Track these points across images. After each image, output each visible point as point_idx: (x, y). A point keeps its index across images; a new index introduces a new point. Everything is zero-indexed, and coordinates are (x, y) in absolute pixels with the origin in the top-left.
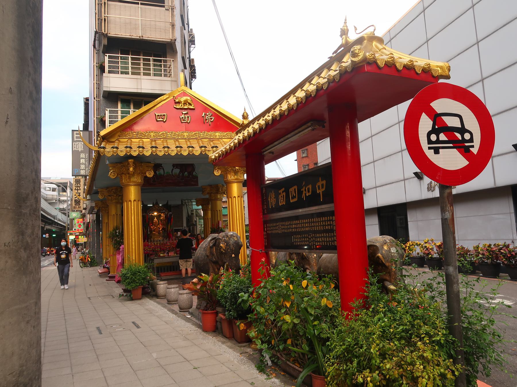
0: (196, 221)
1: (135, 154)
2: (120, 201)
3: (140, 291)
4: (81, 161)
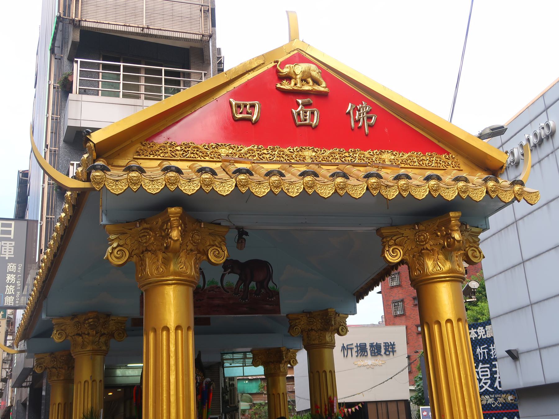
1: (190, 189)
2: (104, 348)
4: (8, 278)
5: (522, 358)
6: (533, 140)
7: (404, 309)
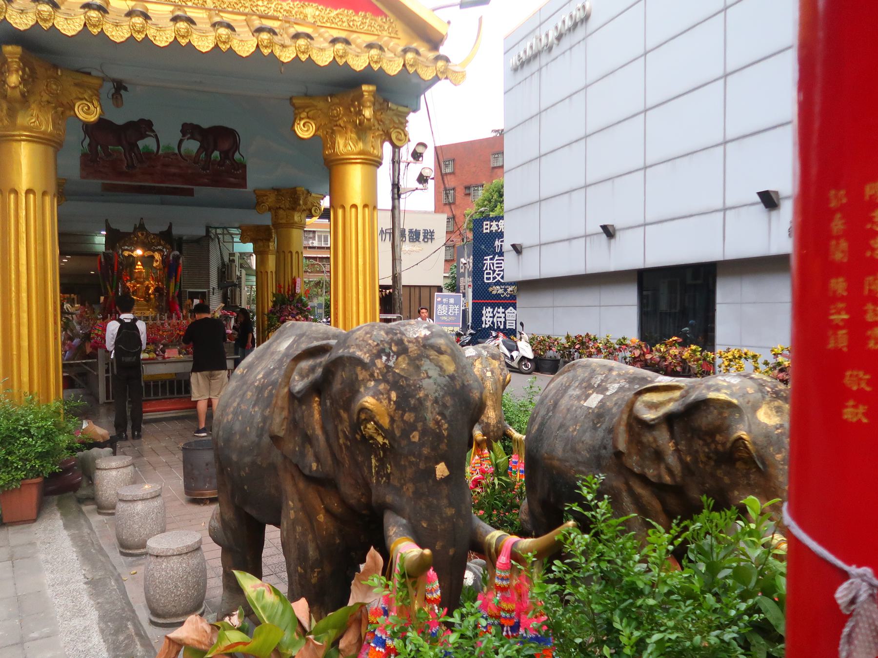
0: (239, 278)
3: (32, 495)
5: (524, 252)
6: (568, 23)
7: (455, 199)
